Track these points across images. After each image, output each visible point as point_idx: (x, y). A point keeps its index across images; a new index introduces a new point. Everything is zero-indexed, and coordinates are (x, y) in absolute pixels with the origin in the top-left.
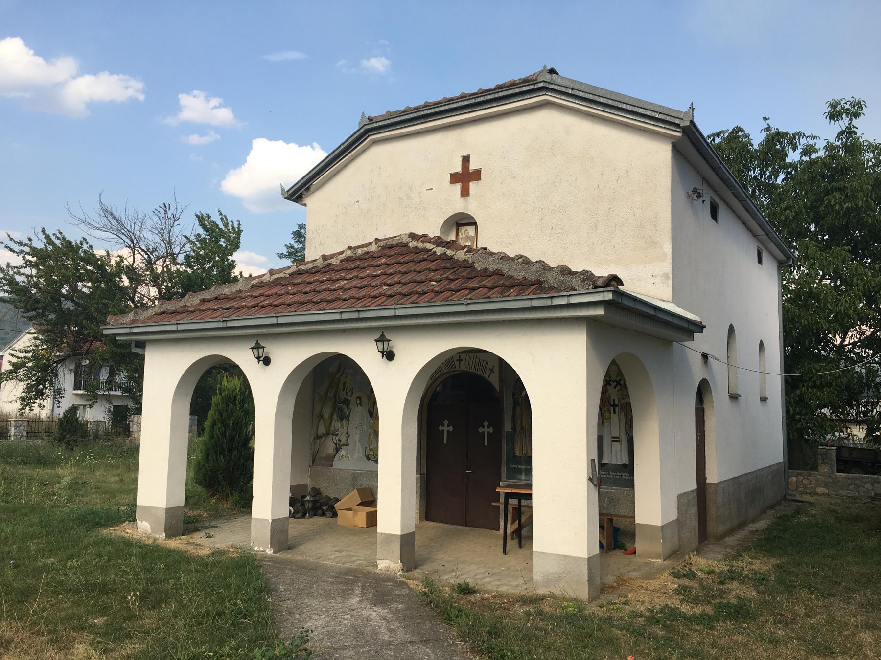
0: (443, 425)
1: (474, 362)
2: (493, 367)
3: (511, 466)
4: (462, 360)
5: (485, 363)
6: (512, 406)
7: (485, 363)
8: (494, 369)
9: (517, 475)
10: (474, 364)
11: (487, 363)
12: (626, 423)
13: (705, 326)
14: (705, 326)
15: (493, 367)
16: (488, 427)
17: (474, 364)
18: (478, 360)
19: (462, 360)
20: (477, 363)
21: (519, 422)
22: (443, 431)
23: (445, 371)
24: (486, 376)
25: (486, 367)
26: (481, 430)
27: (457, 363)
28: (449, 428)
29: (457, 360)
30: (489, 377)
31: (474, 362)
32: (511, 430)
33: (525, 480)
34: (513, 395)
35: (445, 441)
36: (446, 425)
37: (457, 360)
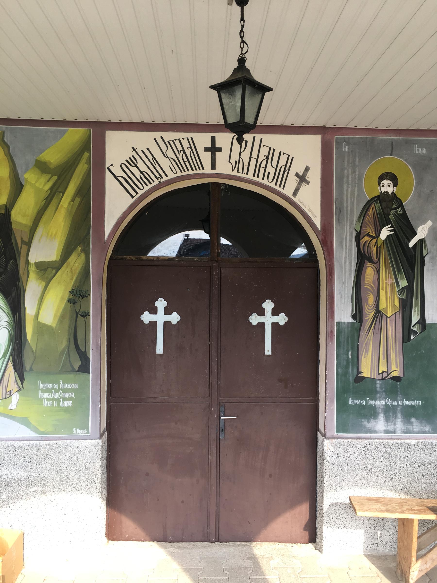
0: (154, 311)
1: (255, 155)
2: (307, 169)
3: (351, 402)
4: (220, 150)
5: (283, 159)
6: (354, 264)
7: (283, 159)
8: (309, 174)
9: (365, 423)
10: (253, 162)
11: (290, 160)
12: (27, 277)
13: (308, 183)
14: (308, 183)
15: (307, 169)
16: (275, 313)
17: (253, 162)
18: (264, 151)
19: (220, 150)
20: (261, 158)
21: (371, 300)
22: (154, 324)
23: (171, 176)
24: (288, 191)
25: (287, 168)
26: (254, 319)
27: (206, 157)
28: (168, 318)
29: (206, 149)
30: (295, 194)
31: (255, 155)
32: (351, 320)
33: (387, 432)
34: (358, 238)
35: (160, 349)
36: (261, 319)
37: (206, 149)
